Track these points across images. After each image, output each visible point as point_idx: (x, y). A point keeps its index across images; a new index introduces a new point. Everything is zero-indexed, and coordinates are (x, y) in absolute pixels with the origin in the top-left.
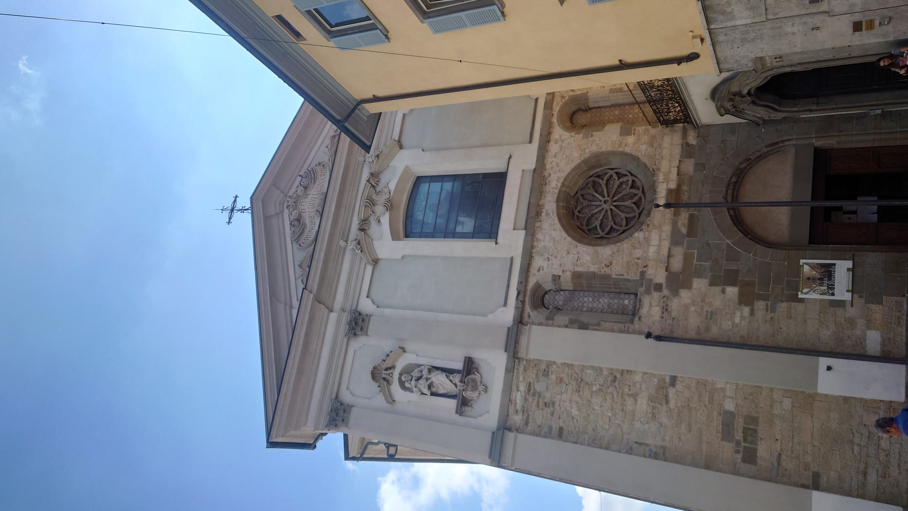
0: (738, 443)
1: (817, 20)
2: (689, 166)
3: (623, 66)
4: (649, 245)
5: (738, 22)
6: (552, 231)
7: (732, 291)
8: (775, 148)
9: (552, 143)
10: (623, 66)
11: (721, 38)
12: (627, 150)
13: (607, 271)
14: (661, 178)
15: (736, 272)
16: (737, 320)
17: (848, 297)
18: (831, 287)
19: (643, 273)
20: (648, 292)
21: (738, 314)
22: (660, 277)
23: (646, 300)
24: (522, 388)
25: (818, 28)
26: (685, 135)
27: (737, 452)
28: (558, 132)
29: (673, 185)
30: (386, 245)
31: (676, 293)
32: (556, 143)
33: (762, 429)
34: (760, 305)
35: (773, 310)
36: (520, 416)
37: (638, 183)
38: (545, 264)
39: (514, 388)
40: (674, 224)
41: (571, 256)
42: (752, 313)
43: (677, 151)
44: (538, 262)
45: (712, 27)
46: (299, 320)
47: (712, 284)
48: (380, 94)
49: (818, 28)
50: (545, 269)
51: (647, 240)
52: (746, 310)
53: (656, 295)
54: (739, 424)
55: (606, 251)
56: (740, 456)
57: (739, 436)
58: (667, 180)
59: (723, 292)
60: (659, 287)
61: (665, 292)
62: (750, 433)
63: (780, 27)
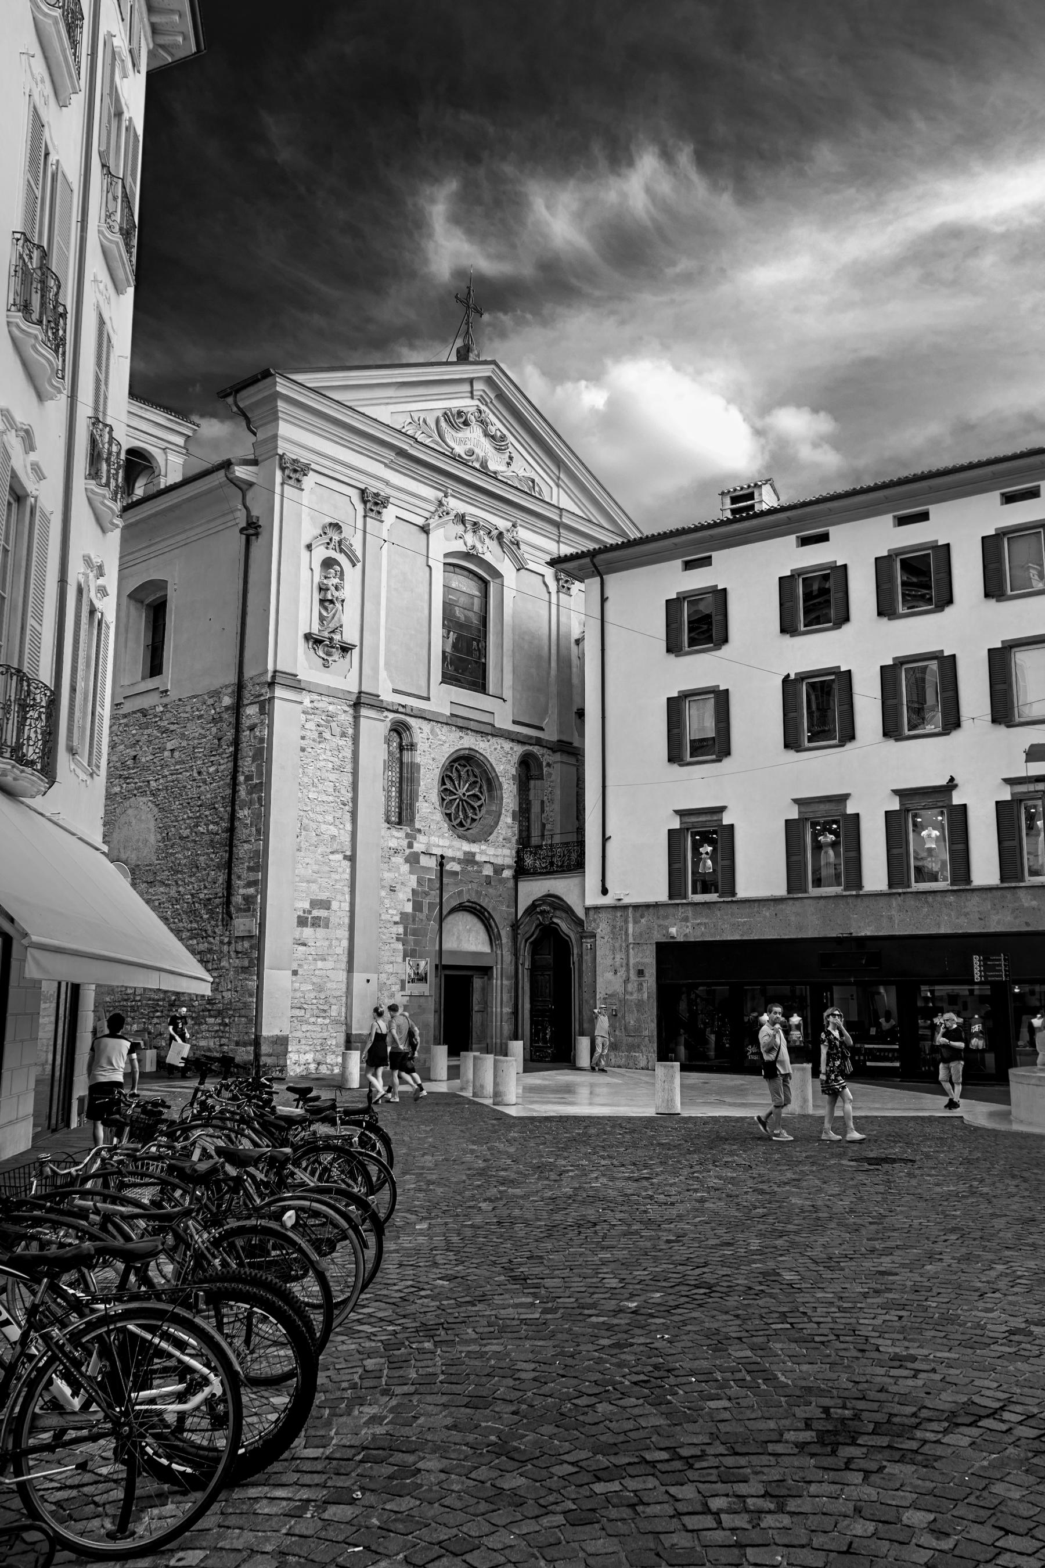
0: (310, 912)
1: (622, 972)
2: (488, 871)
3: (605, 839)
4: (439, 837)
5: (631, 926)
6: (452, 742)
7: (409, 908)
8: (493, 936)
9: (511, 744)
10: (605, 839)
11: (619, 914)
12: (502, 817)
13: (421, 798)
14: (483, 847)
15: (421, 911)
16: (390, 911)
17: (407, 992)
18: (413, 981)
19: (419, 831)
20: (407, 835)
21: (395, 912)
22: (418, 847)
23: (401, 834)
24: (331, 708)
25: (616, 973)
26: (509, 867)
27: (304, 912)
28: (519, 749)
29: (478, 858)
30: (446, 540)
31: (407, 861)
32: (511, 748)
33: (321, 932)
34: (401, 929)
35: (398, 939)
36: (310, 705)
37: (474, 825)
38: (424, 735)
39: (331, 699)
40: (453, 859)
41: (431, 762)
42: (396, 923)
43: (499, 861)
44: (426, 726)
45: (631, 909)
46: (108, 68)
47: (413, 890)
48: (608, 605)
49: (616, 973)
50: (421, 731)
51: (442, 836)
52: (397, 919)
53: (405, 843)
54: (322, 913)
55: (434, 797)
56: (301, 914)
57: (315, 913)
58: (482, 852)
59: (409, 900)
60: (410, 846)
61: (408, 851)
62: (316, 923)
63: (621, 950)
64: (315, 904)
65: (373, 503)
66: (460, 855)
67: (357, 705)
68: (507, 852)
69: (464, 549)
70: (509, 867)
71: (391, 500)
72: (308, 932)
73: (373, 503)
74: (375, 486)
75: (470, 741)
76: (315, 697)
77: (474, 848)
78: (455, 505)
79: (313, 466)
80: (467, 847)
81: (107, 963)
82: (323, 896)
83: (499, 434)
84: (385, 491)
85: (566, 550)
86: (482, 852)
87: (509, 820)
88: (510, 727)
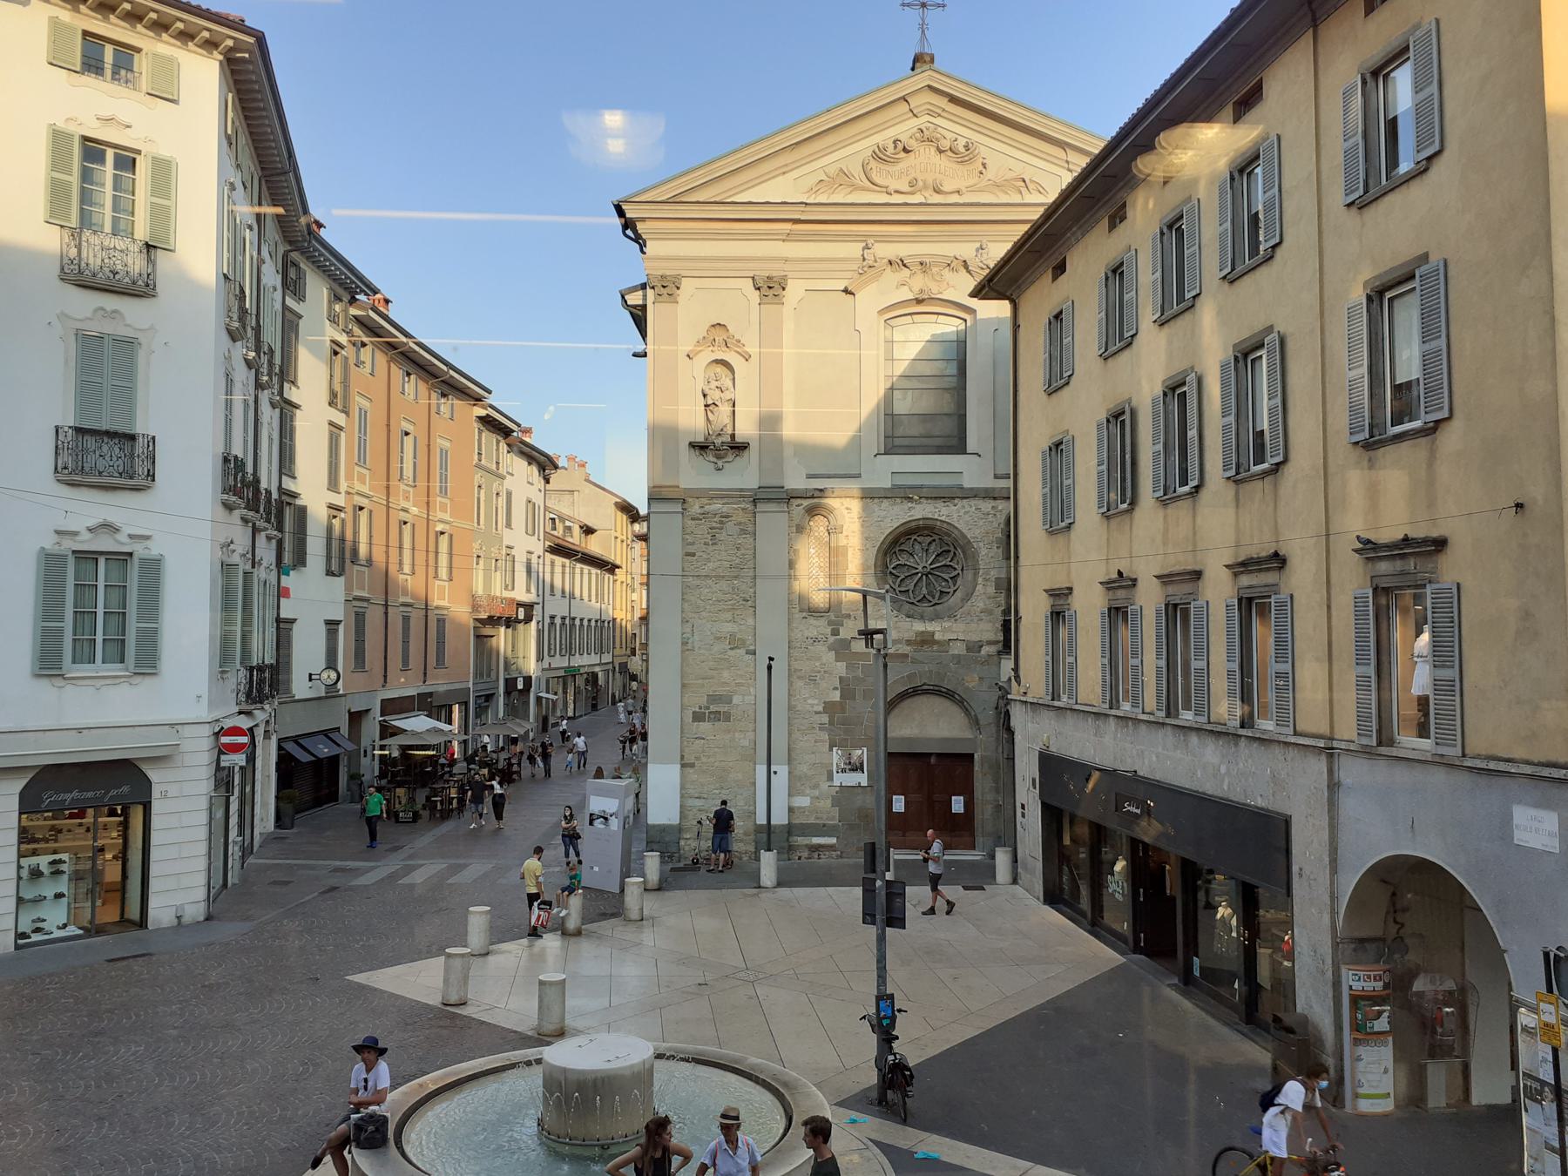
7: (836, 696)
8: (975, 722)
14: (946, 624)
18: (844, 771)
34: (825, 719)
53: (829, 630)
54: (722, 708)
57: (713, 708)
60: (835, 633)
61: (832, 639)
62: (717, 716)
64: (713, 699)
65: (770, 288)
66: (911, 636)
67: (754, 501)
68: (989, 626)
69: (911, 296)
70: (990, 643)
71: (790, 275)
72: (705, 727)
73: (770, 288)
74: (763, 271)
75: (988, 556)
76: (705, 501)
77: (936, 628)
78: (885, 251)
79: (684, 273)
80: (919, 626)
81: (474, 1083)
82: (721, 691)
83: (962, 142)
84: (775, 270)
85: (998, 250)
86: (944, 630)
87: (991, 590)
88: (989, 483)
